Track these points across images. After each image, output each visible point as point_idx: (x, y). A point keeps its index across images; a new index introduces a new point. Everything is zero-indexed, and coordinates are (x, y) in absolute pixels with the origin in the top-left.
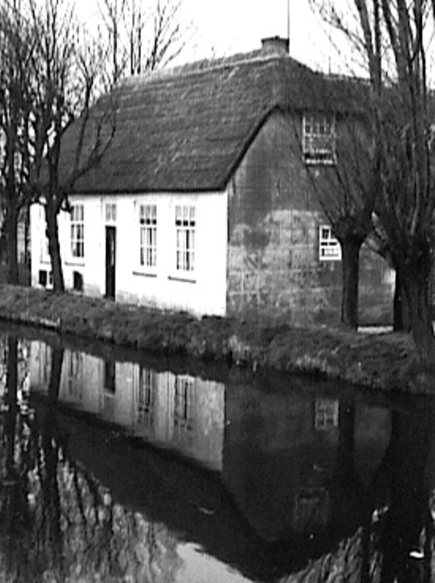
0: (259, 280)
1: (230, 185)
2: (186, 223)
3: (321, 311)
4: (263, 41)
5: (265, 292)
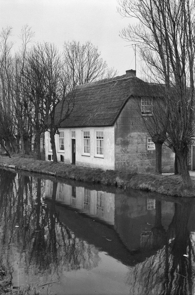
1: (115, 124)
5: (128, 161)
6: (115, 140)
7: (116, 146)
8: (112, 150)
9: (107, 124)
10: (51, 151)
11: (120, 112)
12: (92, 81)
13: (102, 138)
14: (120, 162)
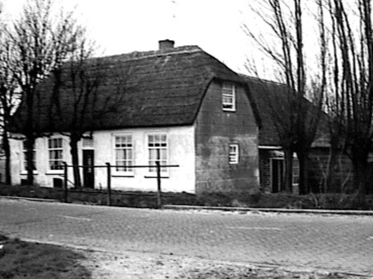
0: (207, 175)
1: (195, 121)
2: (124, 145)
3: (231, 191)
4: (160, 42)
5: (210, 181)
9: (182, 122)
10: (26, 172)
11: (201, 103)
12: (90, 57)
14: (201, 182)
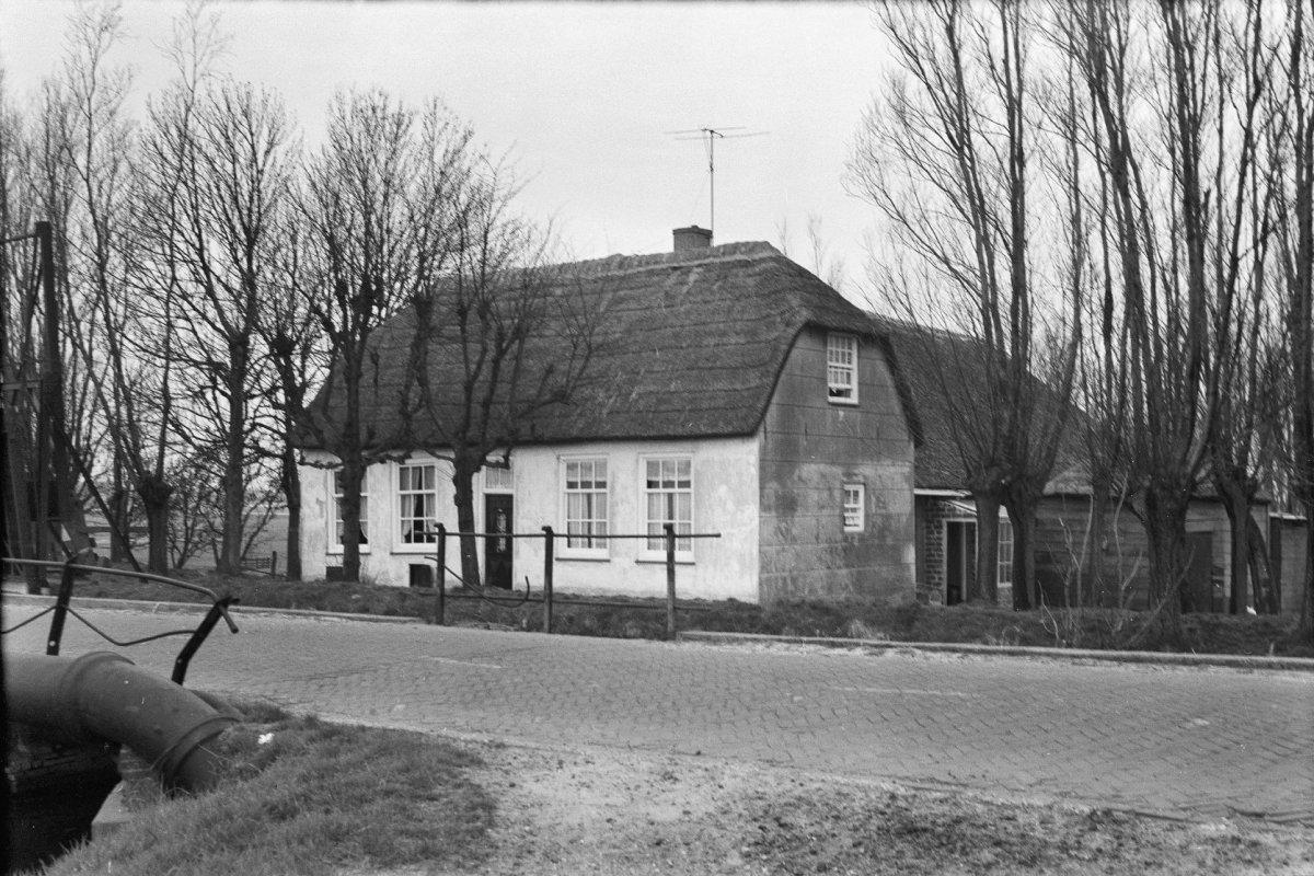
1: (762, 429)
6: (762, 488)
7: (763, 514)
8: (744, 529)
10: (340, 549)
13: (602, 485)
